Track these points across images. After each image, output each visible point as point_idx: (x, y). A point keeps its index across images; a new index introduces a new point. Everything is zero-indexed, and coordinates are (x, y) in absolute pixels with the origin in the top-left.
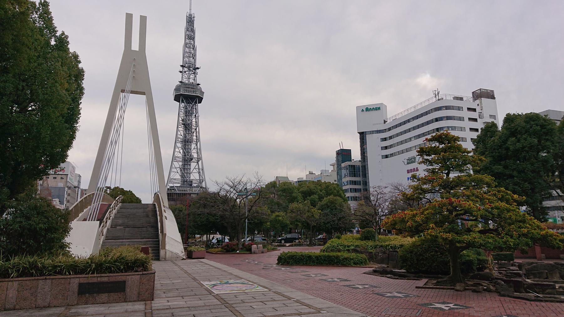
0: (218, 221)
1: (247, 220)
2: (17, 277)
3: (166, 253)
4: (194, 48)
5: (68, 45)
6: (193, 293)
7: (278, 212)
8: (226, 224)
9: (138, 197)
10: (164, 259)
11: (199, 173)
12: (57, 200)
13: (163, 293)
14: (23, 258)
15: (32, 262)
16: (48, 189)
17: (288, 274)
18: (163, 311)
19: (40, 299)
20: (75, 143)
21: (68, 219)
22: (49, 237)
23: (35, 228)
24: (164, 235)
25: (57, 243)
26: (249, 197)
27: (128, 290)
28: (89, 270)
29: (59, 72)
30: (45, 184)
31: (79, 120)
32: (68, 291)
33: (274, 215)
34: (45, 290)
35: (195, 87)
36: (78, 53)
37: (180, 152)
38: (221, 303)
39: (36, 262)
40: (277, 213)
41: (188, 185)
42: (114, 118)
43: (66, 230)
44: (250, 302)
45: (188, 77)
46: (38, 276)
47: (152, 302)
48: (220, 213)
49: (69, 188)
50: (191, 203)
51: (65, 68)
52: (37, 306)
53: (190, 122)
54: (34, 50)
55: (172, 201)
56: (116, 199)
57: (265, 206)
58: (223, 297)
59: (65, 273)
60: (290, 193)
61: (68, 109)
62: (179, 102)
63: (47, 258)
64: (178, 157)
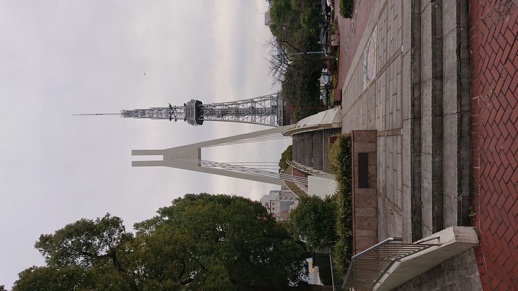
0: (307, 80)
1: (308, 53)
2: (352, 230)
3: (335, 123)
4: (152, 110)
5: (167, 208)
6: (373, 97)
7: (300, 21)
8: (311, 73)
9: (287, 148)
10: (341, 124)
11: (264, 100)
12: (290, 206)
13: (370, 123)
14: (338, 227)
15: (341, 221)
16: (282, 213)
17: (362, 6)
18: (387, 122)
19: (370, 214)
20: (245, 197)
21: (306, 198)
22: (321, 210)
23: (314, 220)
24: (320, 126)
25: (326, 205)
26: (286, 52)
27: (366, 151)
28: (348, 181)
29: (190, 212)
30: (279, 215)
31: (227, 195)
32: (365, 196)
33: (303, 25)
34: (363, 211)
35: (188, 108)
36: (173, 199)
37: (248, 118)
38: (385, 71)
39: (341, 219)
40: (301, 22)
41: (276, 109)
42: (223, 170)
43: (316, 199)
44: (387, 43)
45: (179, 114)
46: (352, 217)
47: (378, 131)
48: (301, 79)
49: (281, 198)
50: (292, 105)
51: (186, 208)
52: (376, 216)
53: (220, 111)
54: (175, 231)
55: (290, 121)
56: (289, 164)
57: (294, 35)
58: (379, 69)
59: (350, 198)
60: (281, 9)
61: (219, 203)
62: (203, 120)
63: (338, 212)
64: (252, 119)
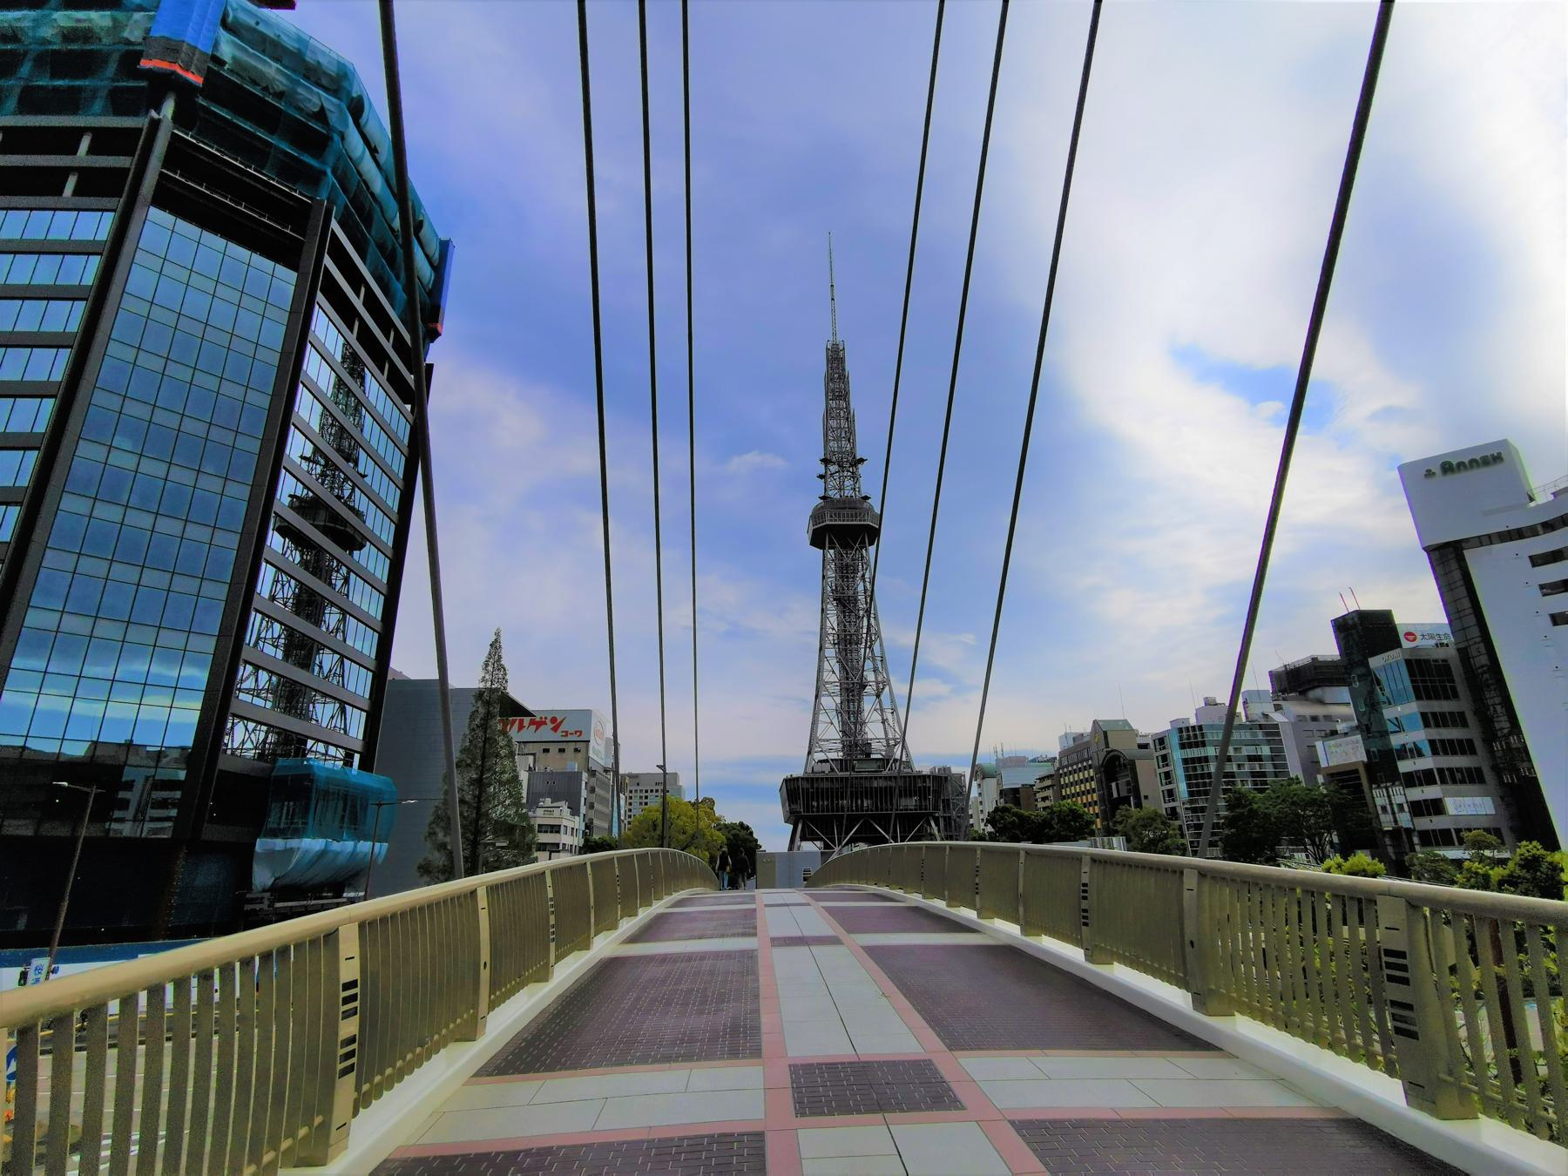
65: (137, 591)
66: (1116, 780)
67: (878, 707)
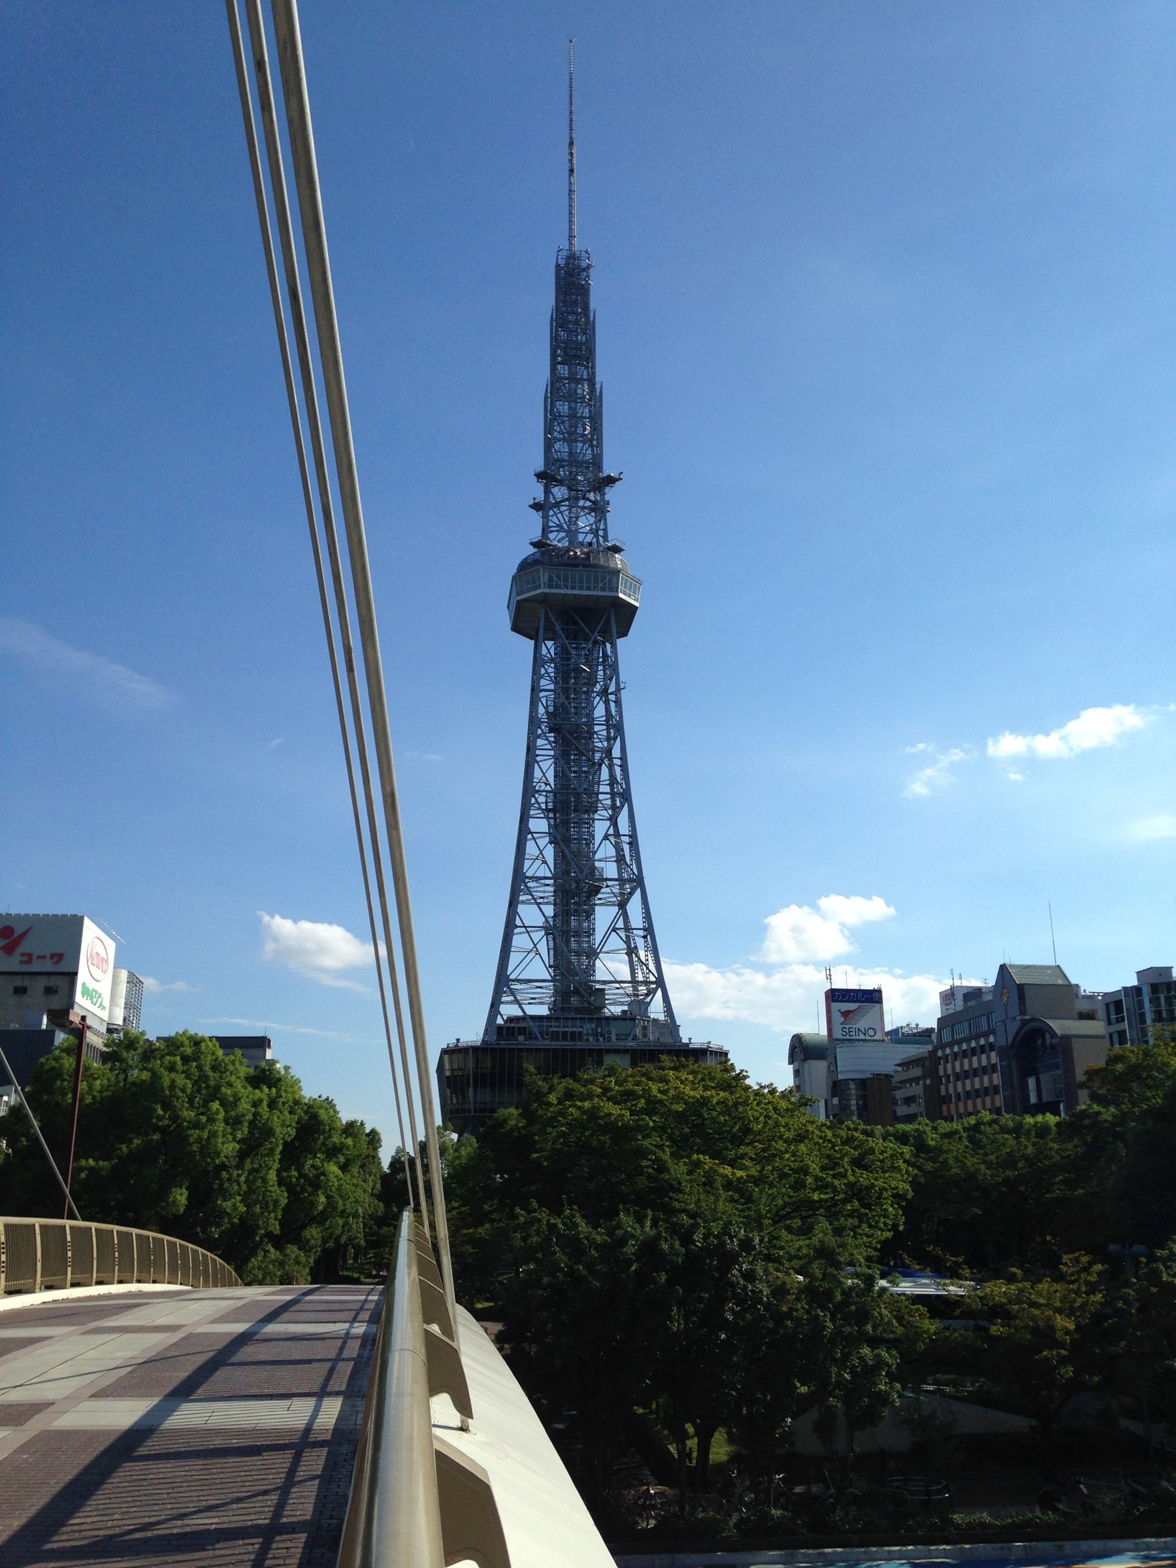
11: (631, 951)
65: (571, 237)
66: (1034, 1072)
67: (620, 924)
